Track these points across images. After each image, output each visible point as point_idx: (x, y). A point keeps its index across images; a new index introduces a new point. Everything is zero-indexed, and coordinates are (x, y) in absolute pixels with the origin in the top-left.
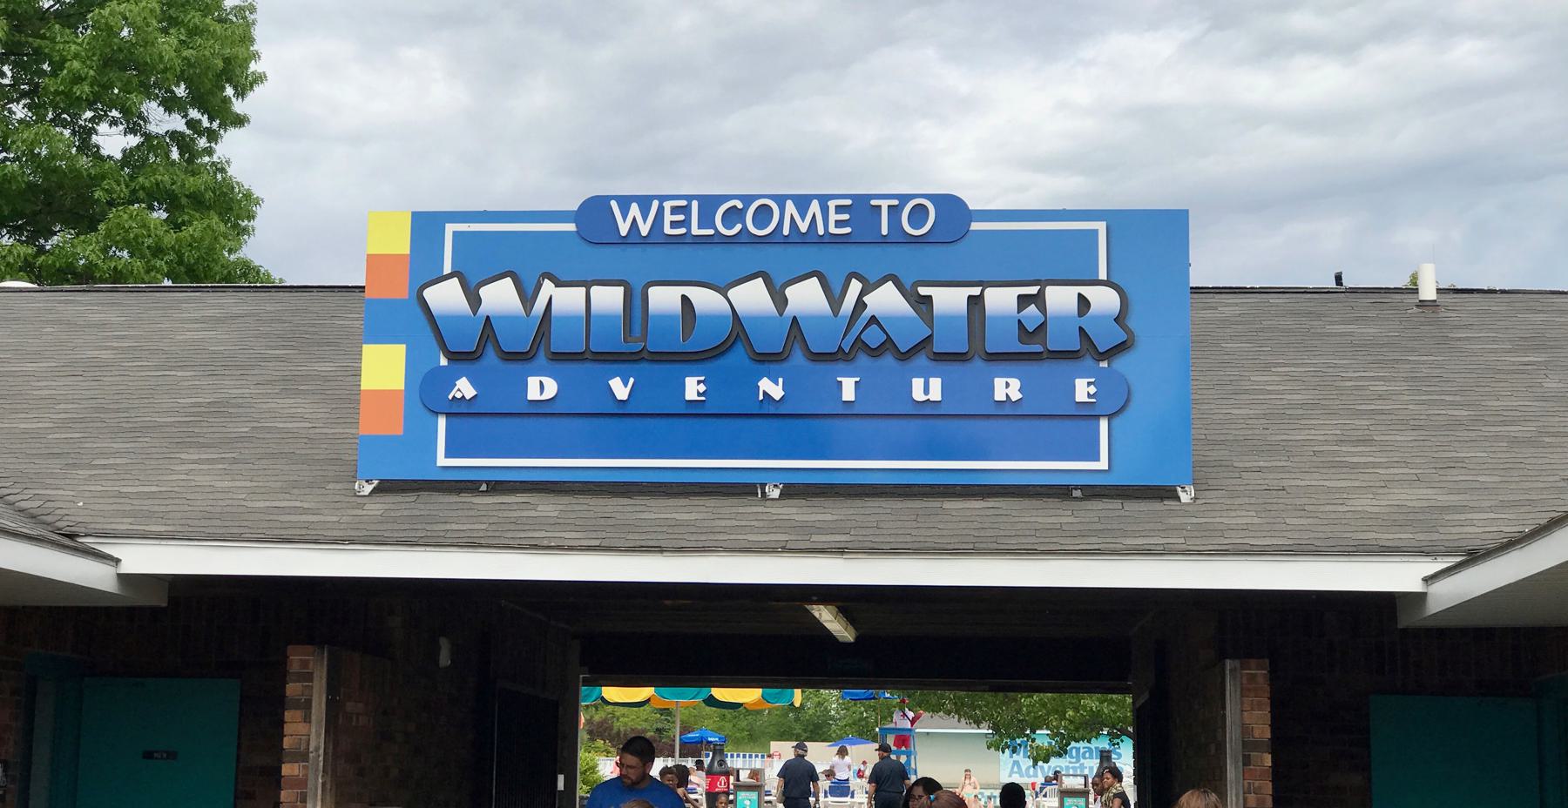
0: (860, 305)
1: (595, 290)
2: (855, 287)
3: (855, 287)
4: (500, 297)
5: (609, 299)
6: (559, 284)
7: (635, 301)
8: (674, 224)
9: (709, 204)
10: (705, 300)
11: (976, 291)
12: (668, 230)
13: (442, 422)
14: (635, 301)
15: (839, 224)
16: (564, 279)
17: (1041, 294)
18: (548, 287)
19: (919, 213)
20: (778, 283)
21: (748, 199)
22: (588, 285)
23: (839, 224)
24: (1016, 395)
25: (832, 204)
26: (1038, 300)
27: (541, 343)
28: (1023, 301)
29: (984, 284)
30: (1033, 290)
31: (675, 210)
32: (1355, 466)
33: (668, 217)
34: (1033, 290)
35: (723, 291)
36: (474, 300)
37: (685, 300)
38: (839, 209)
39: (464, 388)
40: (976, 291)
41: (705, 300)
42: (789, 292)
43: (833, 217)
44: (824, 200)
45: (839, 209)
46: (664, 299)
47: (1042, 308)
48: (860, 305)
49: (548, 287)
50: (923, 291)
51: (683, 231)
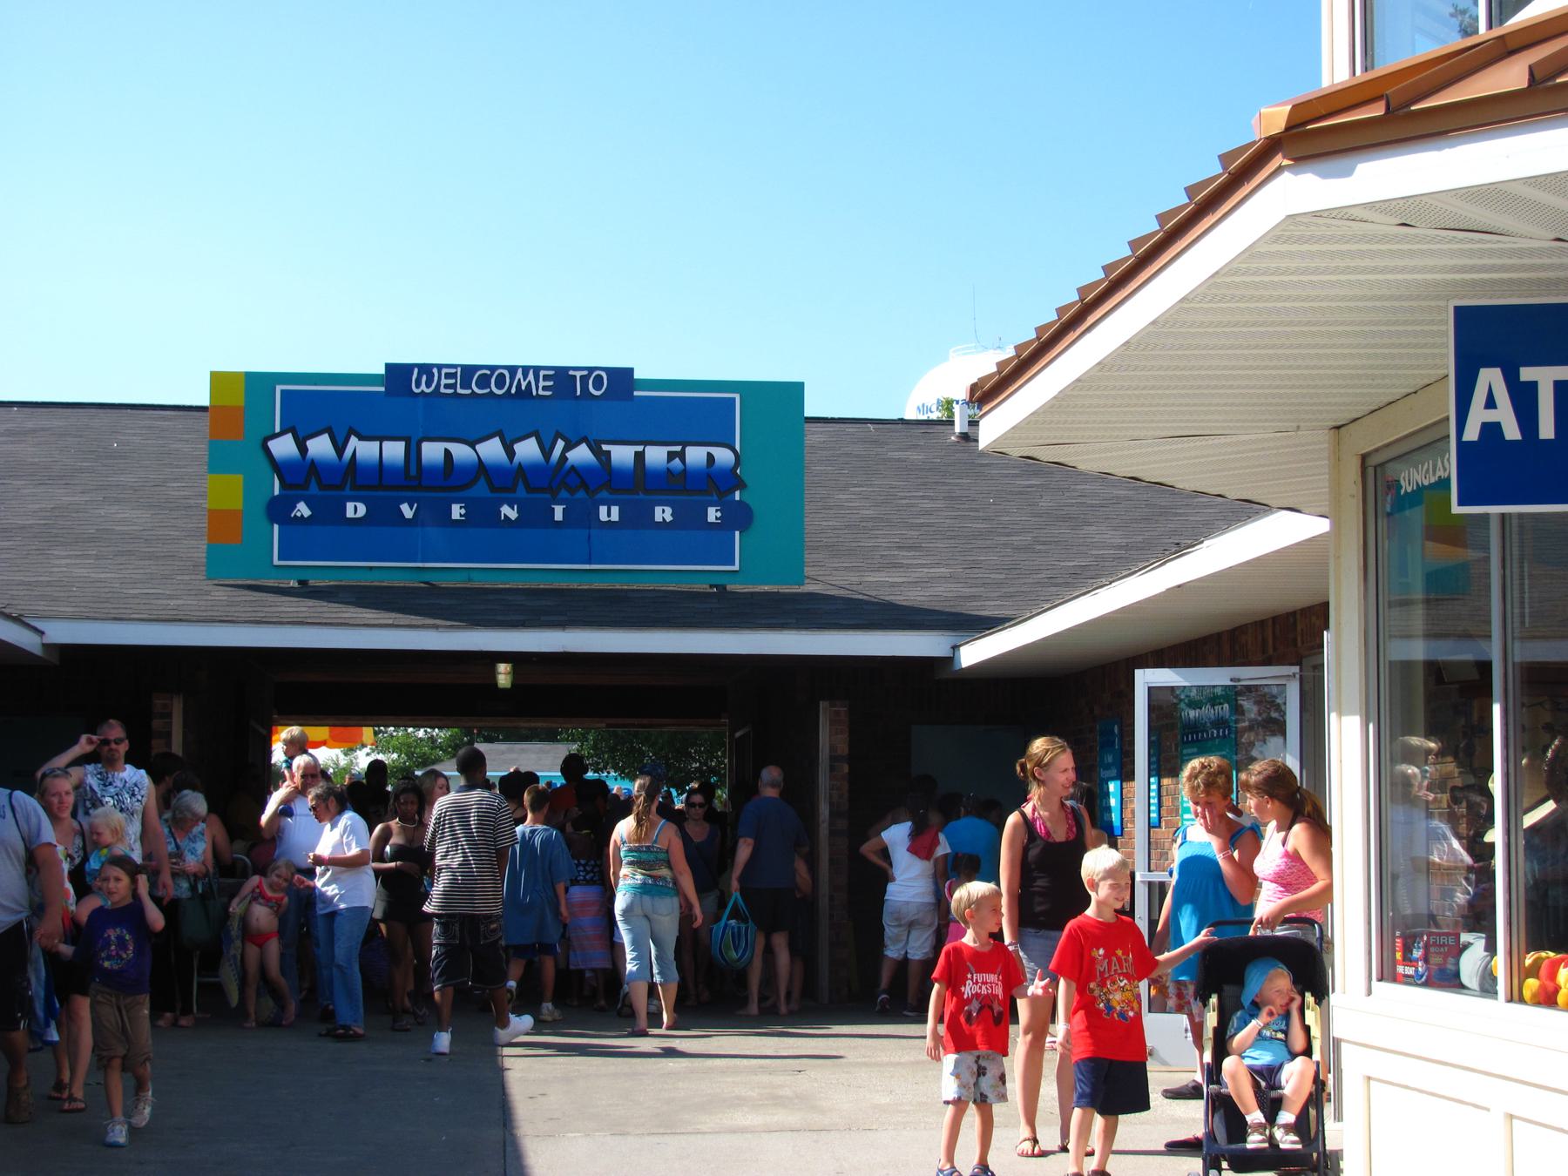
0: (563, 458)
1: (385, 444)
2: (560, 444)
3: (560, 444)
4: (320, 447)
5: (395, 451)
6: (361, 438)
7: (413, 452)
8: (447, 386)
9: (468, 371)
10: (461, 452)
11: (640, 448)
12: (442, 390)
13: (276, 527)
14: (413, 452)
15: (544, 388)
16: (364, 434)
17: (683, 450)
18: (353, 441)
19: (598, 382)
20: (301, 435)
21: (493, 368)
22: (381, 439)
23: (544, 388)
24: (669, 518)
25: (542, 373)
26: (682, 455)
27: (353, 478)
28: (671, 456)
29: (646, 443)
30: (678, 448)
31: (448, 376)
32: (909, 566)
33: (444, 381)
34: (678, 448)
35: (472, 445)
36: (511, 453)
37: (447, 452)
38: (546, 378)
39: (303, 509)
40: (640, 448)
41: (461, 452)
42: (309, 443)
43: (542, 384)
44: (537, 369)
45: (546, 378)
46: (432, 452)
47: (683, 460)
48: (563, 458)
49: (353, 441)
50: (605, 447)
51: (450, 391)
